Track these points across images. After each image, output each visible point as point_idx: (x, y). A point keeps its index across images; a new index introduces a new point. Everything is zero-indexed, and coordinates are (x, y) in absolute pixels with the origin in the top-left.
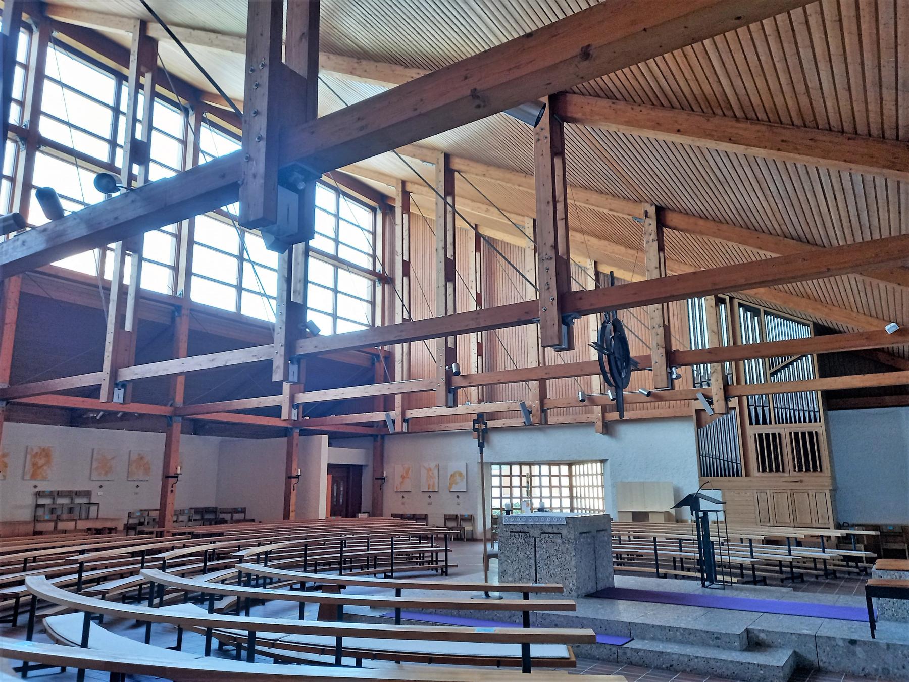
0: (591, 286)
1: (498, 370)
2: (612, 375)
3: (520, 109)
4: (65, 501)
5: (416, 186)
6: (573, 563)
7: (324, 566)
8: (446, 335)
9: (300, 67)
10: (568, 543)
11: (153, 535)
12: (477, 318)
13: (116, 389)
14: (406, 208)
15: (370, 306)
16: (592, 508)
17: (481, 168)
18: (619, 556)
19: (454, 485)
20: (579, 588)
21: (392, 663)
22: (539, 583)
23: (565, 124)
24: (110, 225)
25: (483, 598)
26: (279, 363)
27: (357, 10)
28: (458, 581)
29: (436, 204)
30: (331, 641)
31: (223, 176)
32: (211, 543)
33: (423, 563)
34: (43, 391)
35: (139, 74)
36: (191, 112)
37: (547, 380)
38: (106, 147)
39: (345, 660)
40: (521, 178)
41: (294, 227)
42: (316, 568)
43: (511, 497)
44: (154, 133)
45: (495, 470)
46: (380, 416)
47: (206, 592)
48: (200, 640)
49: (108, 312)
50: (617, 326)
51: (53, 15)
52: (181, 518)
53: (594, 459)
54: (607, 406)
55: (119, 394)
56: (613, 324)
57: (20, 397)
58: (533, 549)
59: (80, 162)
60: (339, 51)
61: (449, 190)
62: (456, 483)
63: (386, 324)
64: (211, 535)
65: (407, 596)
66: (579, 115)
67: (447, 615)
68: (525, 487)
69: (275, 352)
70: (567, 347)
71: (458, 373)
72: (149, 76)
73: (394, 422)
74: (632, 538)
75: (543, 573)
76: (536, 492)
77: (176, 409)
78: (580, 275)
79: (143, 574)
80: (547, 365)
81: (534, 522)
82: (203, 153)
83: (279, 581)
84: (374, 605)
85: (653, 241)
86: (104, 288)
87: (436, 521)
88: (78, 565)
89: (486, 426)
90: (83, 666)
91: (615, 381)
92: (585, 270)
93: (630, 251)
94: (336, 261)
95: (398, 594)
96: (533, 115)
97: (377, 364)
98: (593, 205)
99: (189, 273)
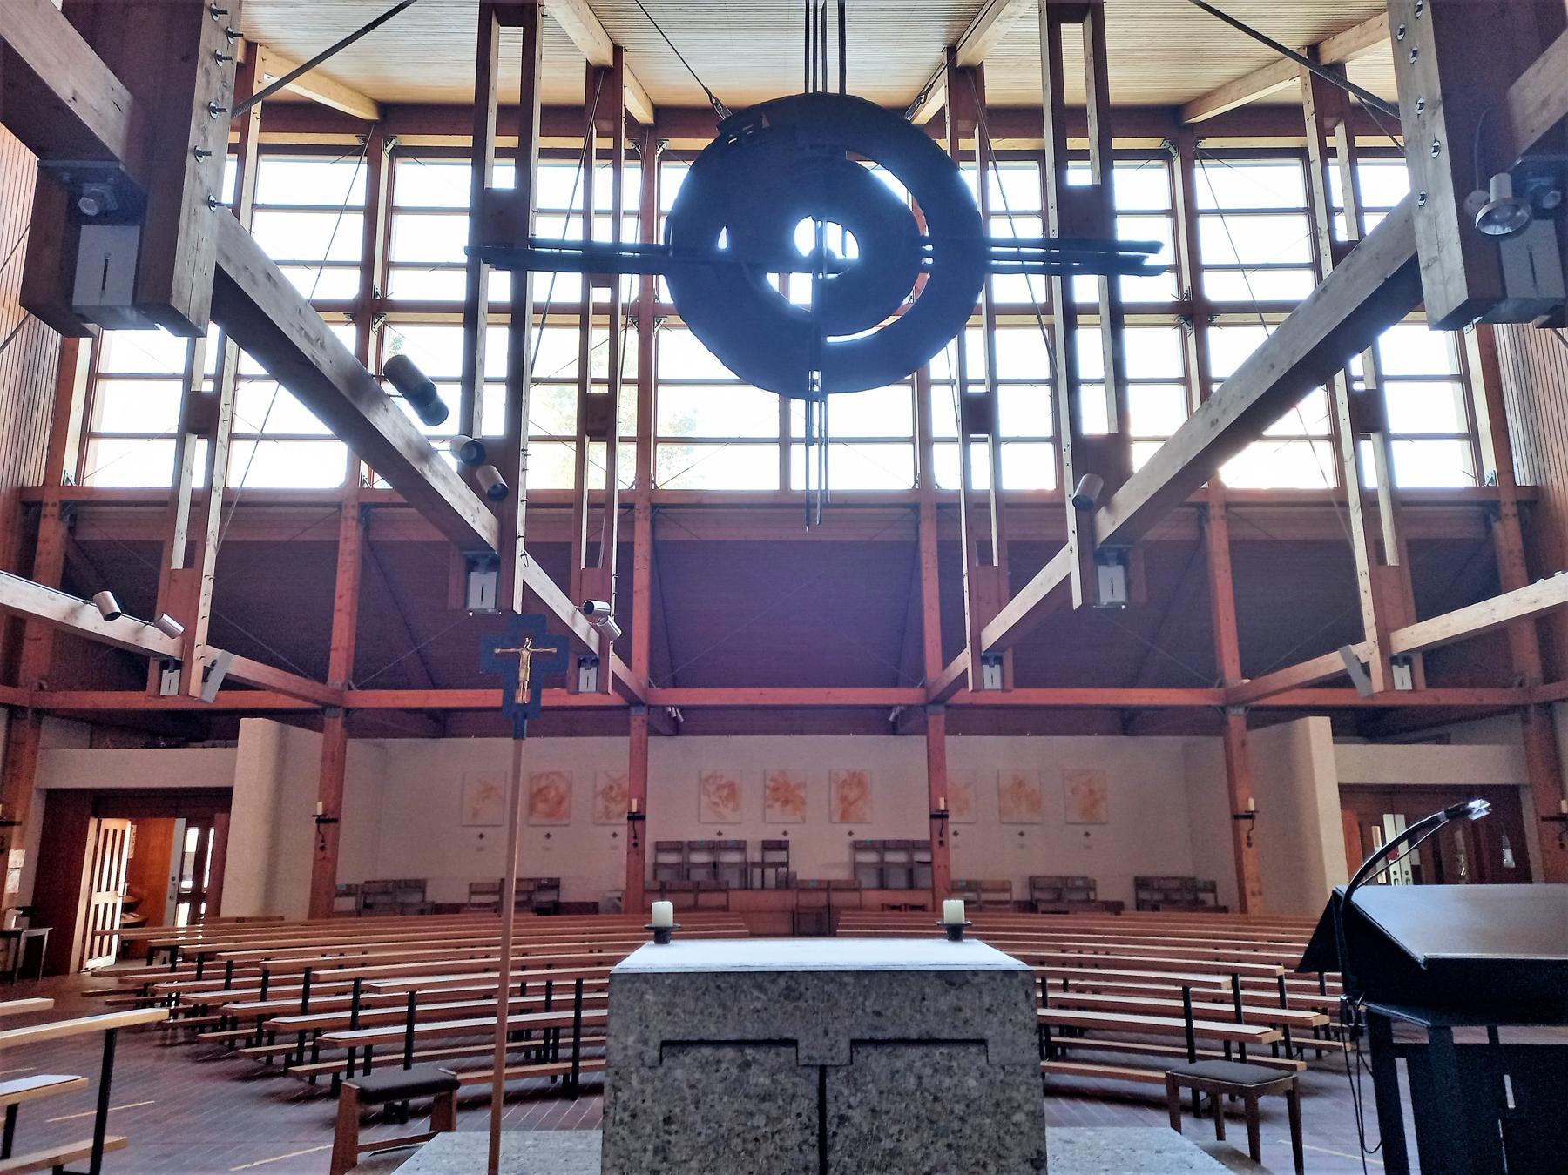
13: (1395, 667)
15: (1458, 386)
35: (1323, 133)
57: (1257, 698)
72: (1340, 130)
73: (1366, 668)
97: (1497, 526)
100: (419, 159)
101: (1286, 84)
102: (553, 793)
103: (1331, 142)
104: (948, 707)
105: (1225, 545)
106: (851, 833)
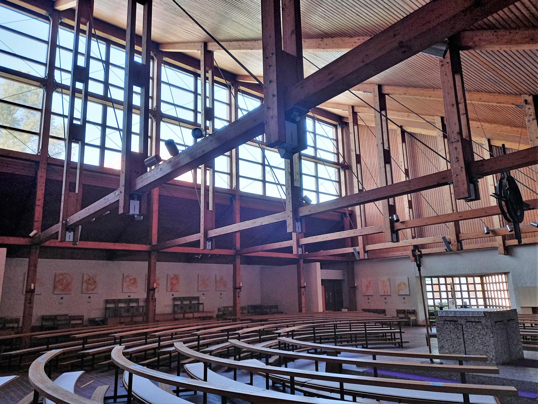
0: (487, 156)
1: (424, 217)
2: (510, 215)
3: (432, 48)
4: (187, 302)
5: (361, 108)
6: (492, 342)
7: (325, 340)
8: (388, 198)
9: (291, 50)
10: (487, 329)
11: (232, 321)
12: (409, 185)
14: (355, 122)
15: (337, 184)
16: (501, 305)
17: (402, 90)
18: (525, 337)
19: (401, 291)
20: (497, 358)
21: (375, 401)
22: (468, 354)
23: (461, 52)
24: (201, 155)
25: (429, 363)
26: (290, 222)
27: (320, 9)
28: (411, 351)
29: (375, 117)
30: (337, 385)
31: (255, 120)
32: (261, 326)
33: (386, 340)
34: (173, 245)
35: (206, 72)
36: (232, 88)
37: (460, 221)
38: (192, 114)
39: (346, 397)
40: (431, 92)
41: (295, 144)
42: (321, 341)
43: (441, 299)
44: (215, 102)
45: (428, 281)
46: (350, 250)
47: (262, 352)
48: (263, 380)
49: (200, 201)
50: (512, 181)
51: (163, 49)
52: (244, 312)
53: (500, 272)
54: (506, 236)
55: (209, 244)
56: (507, 180)
58: (462, 333)
59: (181, 124)
60: (310, 37)
61: (383, 107)
62: (403, 290)
63: (349, 194)
64: (261, 321)
65: (380, 360)
66: (470, 44)
67: (406, 373)
68: (450, 291)
69: (287, 216)
70: (475, 198)
71: (398, 220)
72: (210, 72)
73: (358, 253)
74: (534, 325)
75: (470, 348)
76: (458, 295)
77: (237, 251)
78: (478, 148)
79: (230, 342)
80: (459, 211)
81: (461, 314)
82: (241, 109)
83: (301, 348)
84: (359, 364)
85: (533, 119)
86: (197, 188)
87: (391, 313)
88: (197, 337)
89: (421, 253)
90: (206, 391)
91: (512, 218)
92: (481, 145)
93: (514, 129)
94: (316, 160)
95: (374, 358)
96: (442, 50)
97: (345, 219)
98: (484, 101)
99: (238, 176)
100: (171, 68)
101: (195, 51)
102: (65, 281)
103: (207, 75)
104: (41, 247)
105: (44, 180)
106: (173, 295)
